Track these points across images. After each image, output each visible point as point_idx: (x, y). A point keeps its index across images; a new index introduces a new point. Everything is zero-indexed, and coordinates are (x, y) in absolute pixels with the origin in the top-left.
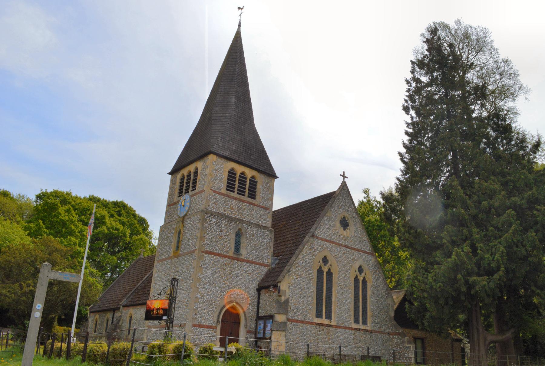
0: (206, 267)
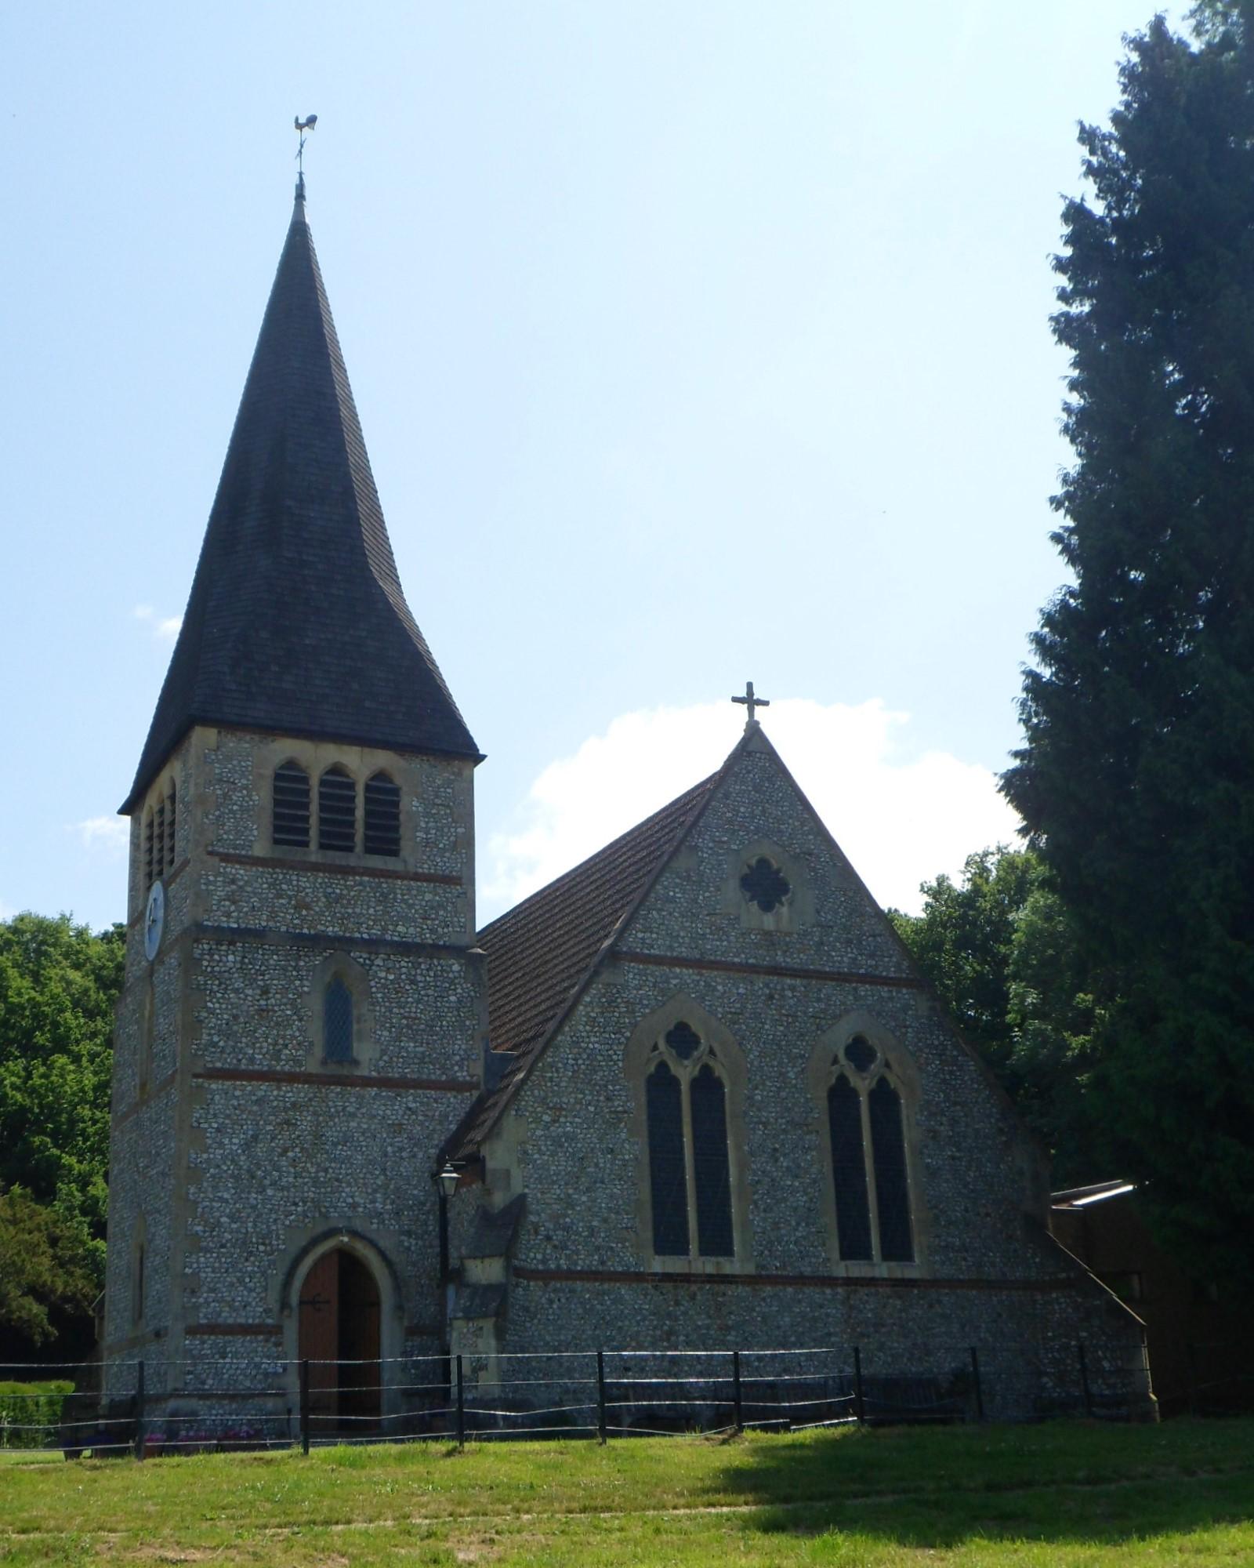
0: (215, 1125)
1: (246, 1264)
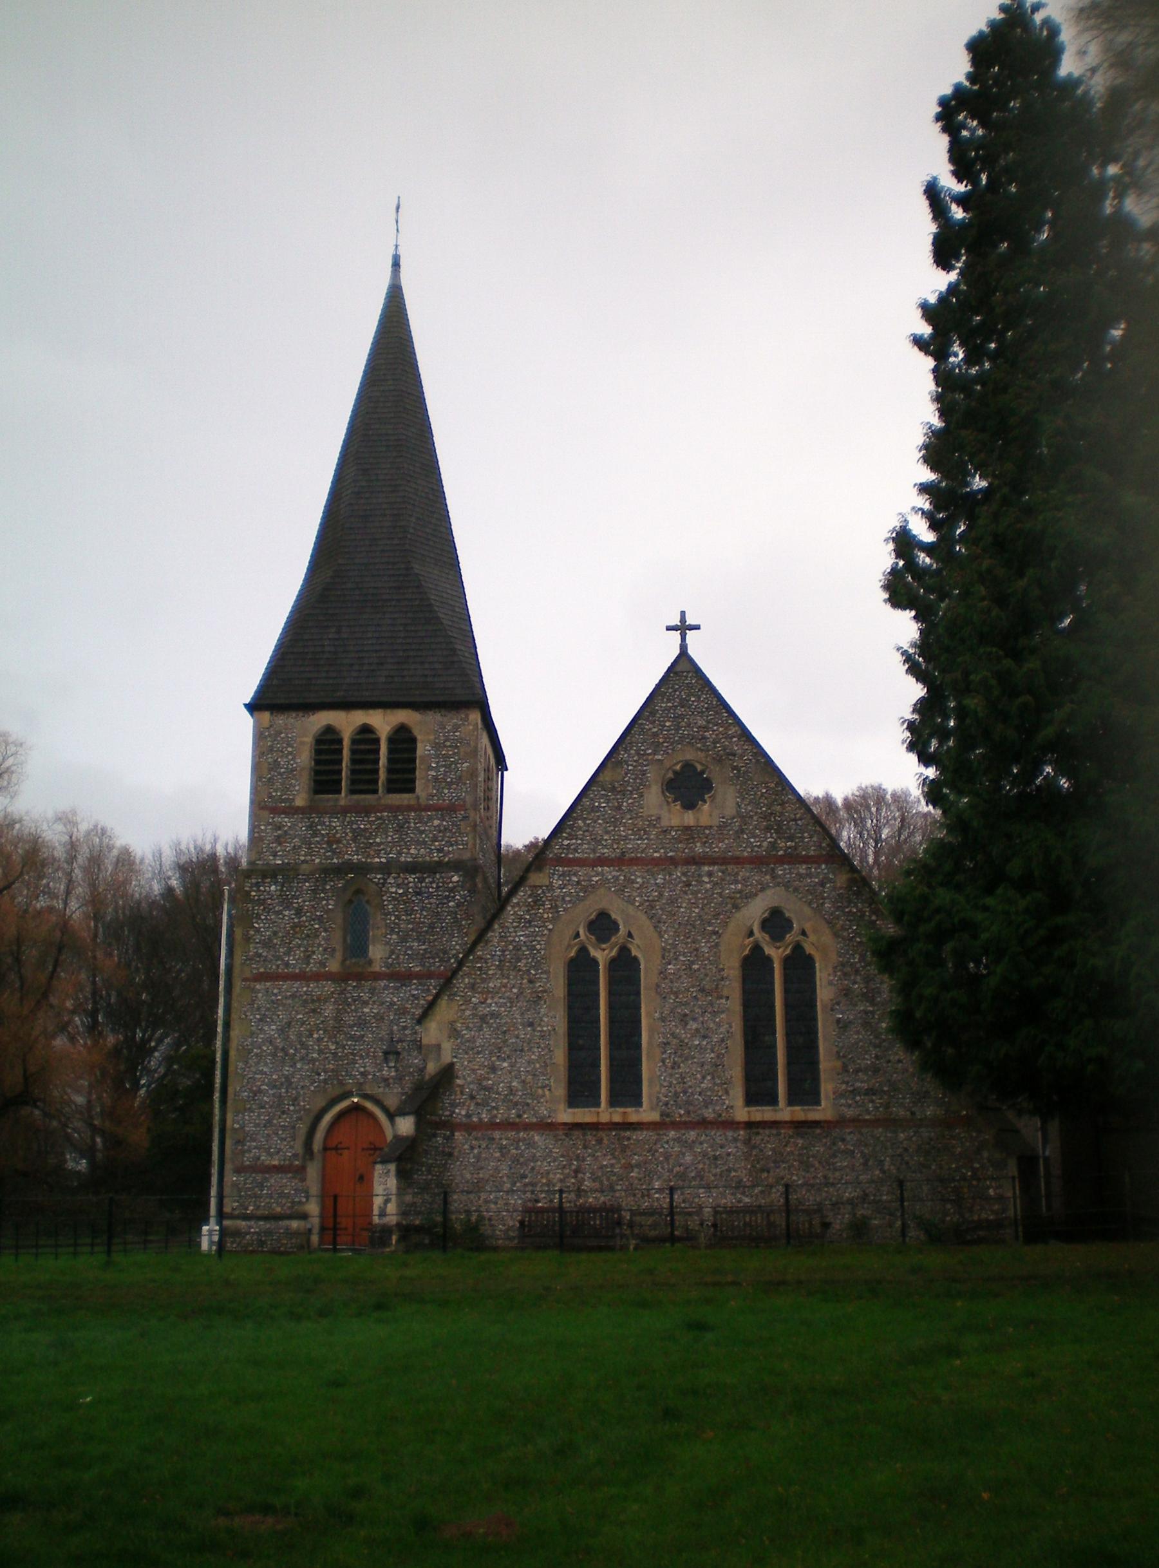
0: (258, 1016)
1: (280, 1120)
